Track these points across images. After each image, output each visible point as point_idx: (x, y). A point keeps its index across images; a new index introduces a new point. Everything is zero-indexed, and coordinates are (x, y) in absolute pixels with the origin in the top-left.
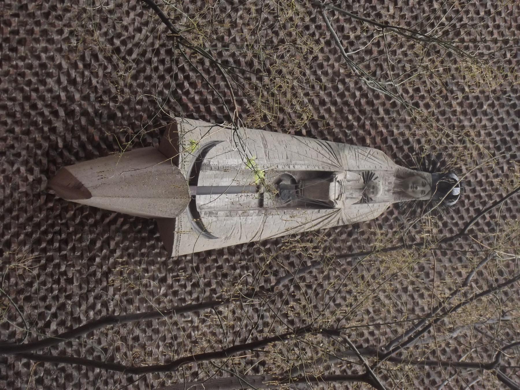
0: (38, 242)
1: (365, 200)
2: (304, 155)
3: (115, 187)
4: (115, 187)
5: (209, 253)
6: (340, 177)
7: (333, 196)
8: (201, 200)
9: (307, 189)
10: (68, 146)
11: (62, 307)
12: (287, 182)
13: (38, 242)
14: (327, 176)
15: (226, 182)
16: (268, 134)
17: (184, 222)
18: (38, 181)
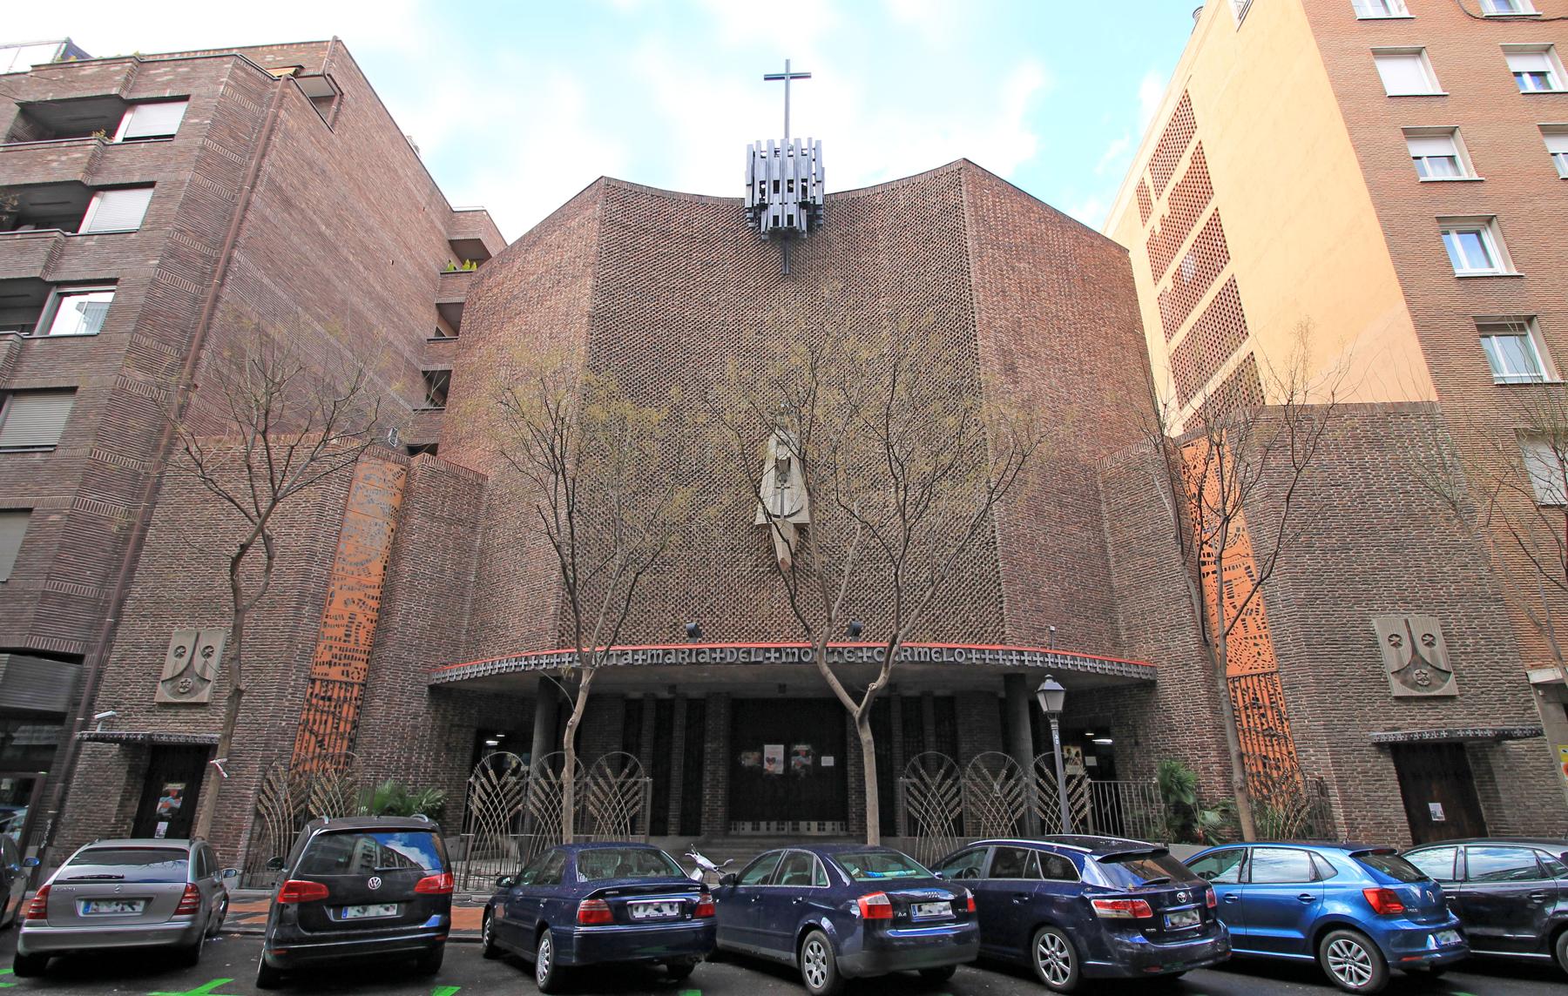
9: (782, 468)
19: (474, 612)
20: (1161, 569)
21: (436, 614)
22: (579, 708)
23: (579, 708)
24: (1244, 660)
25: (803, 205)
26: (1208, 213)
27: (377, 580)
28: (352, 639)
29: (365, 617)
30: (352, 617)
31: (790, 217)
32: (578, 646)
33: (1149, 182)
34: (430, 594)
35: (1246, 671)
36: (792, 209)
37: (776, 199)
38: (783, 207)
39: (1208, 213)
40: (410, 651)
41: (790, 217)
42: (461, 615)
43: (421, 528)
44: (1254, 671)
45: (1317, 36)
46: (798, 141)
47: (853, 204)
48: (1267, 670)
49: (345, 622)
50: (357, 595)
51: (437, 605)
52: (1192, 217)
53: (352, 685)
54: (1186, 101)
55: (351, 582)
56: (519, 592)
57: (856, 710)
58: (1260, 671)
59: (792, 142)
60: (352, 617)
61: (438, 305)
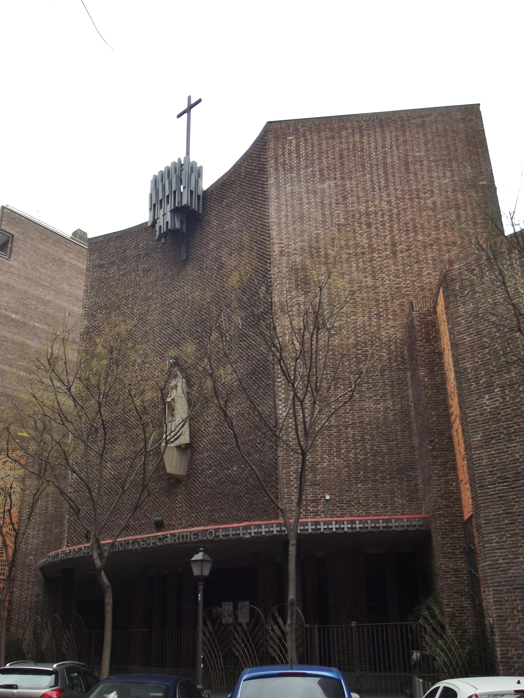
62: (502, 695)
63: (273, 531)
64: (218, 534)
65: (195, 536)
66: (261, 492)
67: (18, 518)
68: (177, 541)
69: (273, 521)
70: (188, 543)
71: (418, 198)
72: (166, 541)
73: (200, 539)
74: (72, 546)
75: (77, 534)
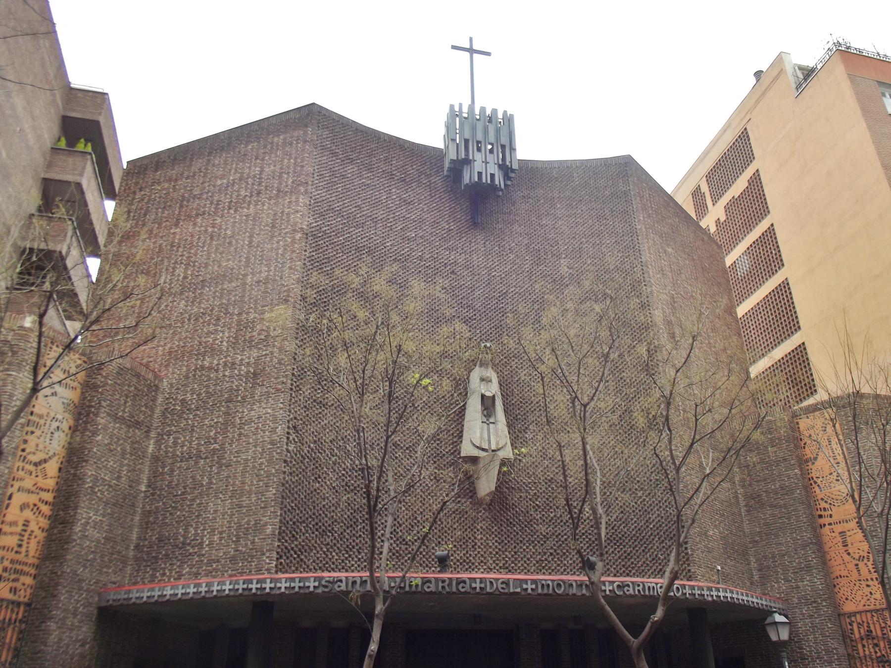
0: (507, 509)
1: (491, 381)
2: (474, 407)
3: (486, 485)
4: (486, 485)
5: (512, 445)
6: (483, 392)
7: (491, 395)
8: (493, 447)
9: (488, 404)
10: (471, 497)
11: (530, 499)
12: (485, 412)
13: (507, 509)
14: (483, 396)
15: (486, 436)
16: (466, 419)
17: (502, 454)
18: (484, 509)
19: (146, 525)
20: (789, 519)
21: (110, 525)
22: (376, 635)
23: (376, 635)
24: (859, 598)
25: (501, 167)
26: (763, 226)
27: (51, 483)
28: (23, 549)
29: (38, 525)
30: (26, 523)
31: (492, 176)
32: (372, 572)
33: (705, 188)
34: (106, 503)
35: (861, 608)
36: (493, 169)
37: (479, 157)
38: (483, 167)
39: (763, 226)
40: (85, 567)
41: (492, 176)
42: (131, 527)
43: (105, 428)
44: (867, 608)
45: (866, 120)
46: (483, 109)
47: (535, 172)
48: (878, 607)
49: (19, 529)
50: (33, 499)
51: (112, 514)
52: (749, 227)
53: (19, 604)
54: (744, 136)
55: (28, 483)
56: (218, 508)
57: (634, 642)
58: (872, 607)
59: (477, 112)
60: (26, 523)
61: (45, 179)
62: (718, 140)
63: (309, 587)
64: (474, 585)
65: (504, 586)
66: (159, 548)
67: (56, 480)
68: (447, 589)
69: (310, 574)
70: (551, 595)
71: (311, 517)
72: (339, 587)
73: (512, 590)
74: (550, 574)
75: (296, 546)
